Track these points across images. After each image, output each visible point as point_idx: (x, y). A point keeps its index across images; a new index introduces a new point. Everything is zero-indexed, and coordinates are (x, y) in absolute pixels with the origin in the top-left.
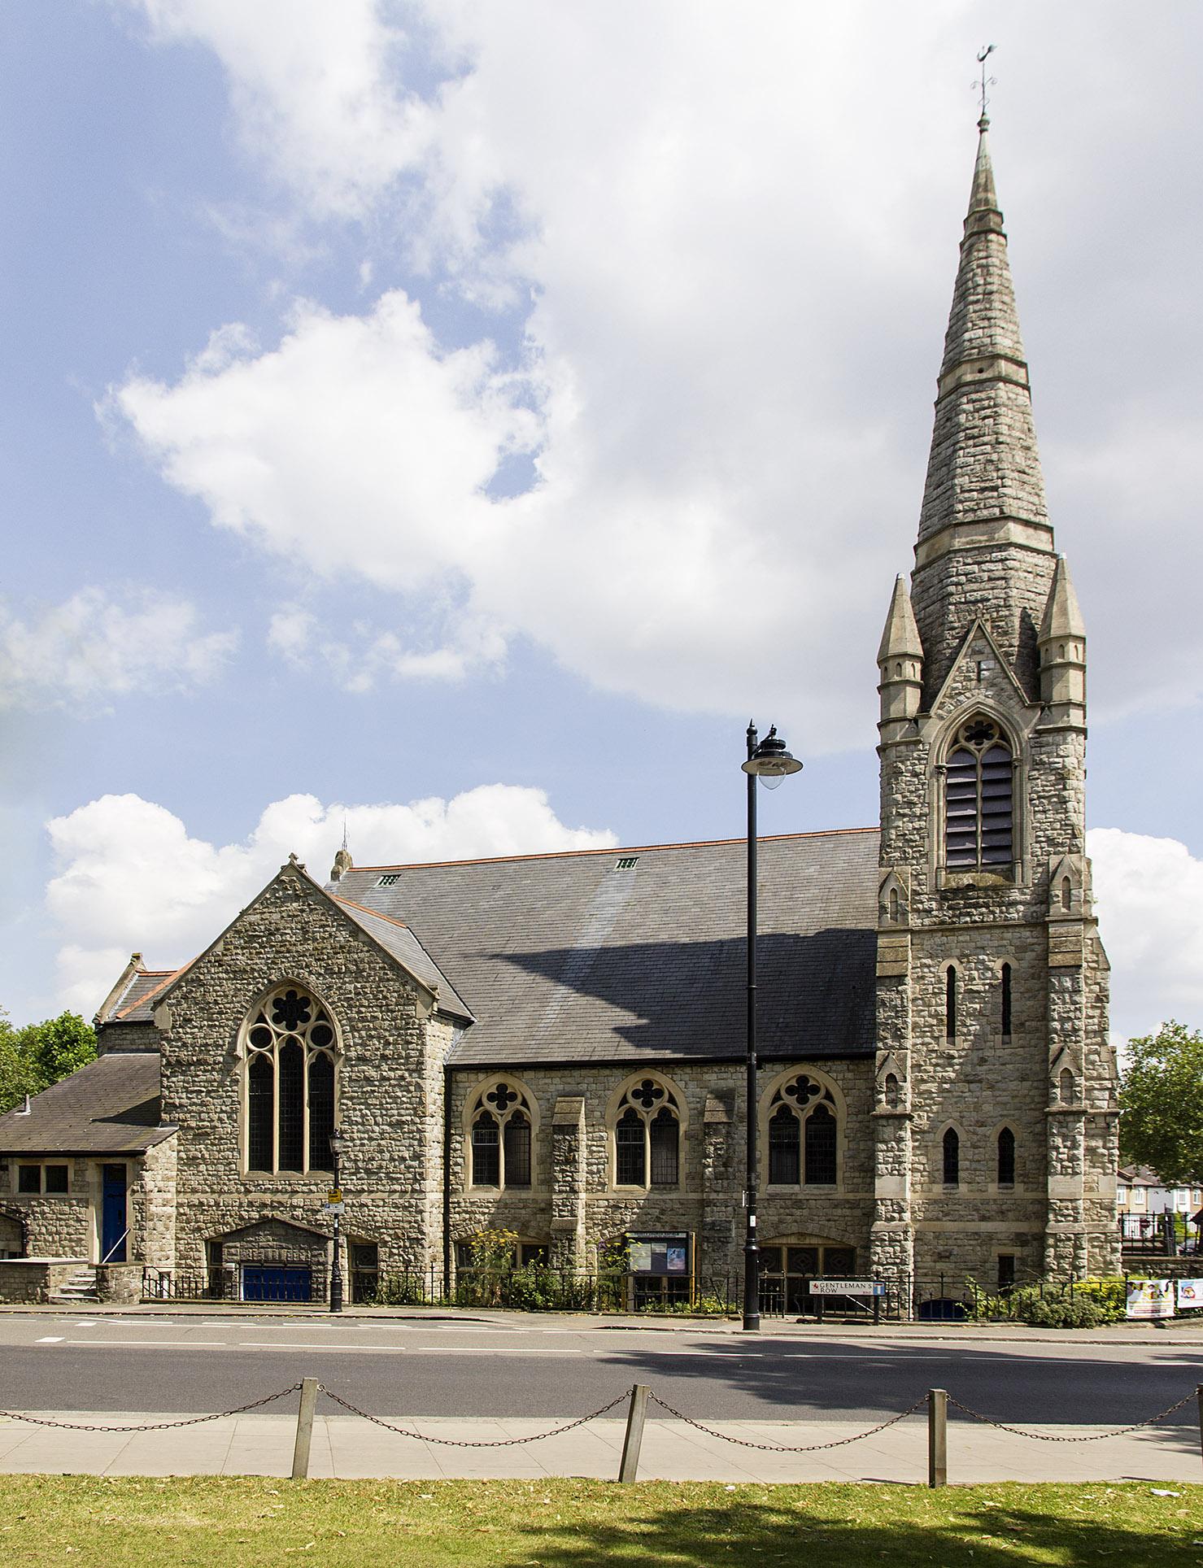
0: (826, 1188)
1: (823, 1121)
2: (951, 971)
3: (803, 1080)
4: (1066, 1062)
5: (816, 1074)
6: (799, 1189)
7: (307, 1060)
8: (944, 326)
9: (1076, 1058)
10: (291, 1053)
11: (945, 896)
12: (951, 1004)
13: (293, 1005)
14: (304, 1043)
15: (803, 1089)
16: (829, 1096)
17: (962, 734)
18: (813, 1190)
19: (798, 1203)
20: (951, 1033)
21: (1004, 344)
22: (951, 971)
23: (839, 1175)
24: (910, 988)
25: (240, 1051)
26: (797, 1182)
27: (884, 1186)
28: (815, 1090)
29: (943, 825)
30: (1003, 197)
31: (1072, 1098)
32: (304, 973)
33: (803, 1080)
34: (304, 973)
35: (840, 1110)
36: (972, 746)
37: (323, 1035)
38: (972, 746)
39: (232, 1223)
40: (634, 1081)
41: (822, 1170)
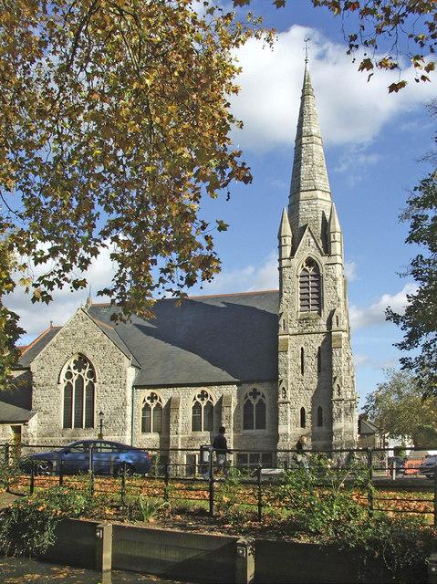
0: (263, 430)
1: (261, 405)
2: (302, 349)
3: (255, 390)
4: (337, 382)
5: (260, 388)
6: (254, 432)
7: (86, 384)
8: (297, 123)
9: (341, 379)
10: (80, 380)
11: (300, 321)
12: (302, 362)
13: (82, 361)
14: (85, 377)
15: (255, 393)
16: (263, 396)
17: (305, 264)
18: (259, 431)
19: (254, 437)
20: (302, 373)
21: (116, 265)
22: (302, 349)
23: (267, 425)
24: (289, 355)
25: (61, 381)
26: (253, 428)
27: (282, 429)
28: (259, 393)
29: (299, 296)
30: (313, 82)
31: (340, 394)
32: (85, 350)
33: (255, 390)
34: (85, 350)
35: (267, 401)
36: (307, 268)
37: (92, 374)
38: (307, 268)
39: (323, 272)
40: (198, 391)
41: (261, 425)
